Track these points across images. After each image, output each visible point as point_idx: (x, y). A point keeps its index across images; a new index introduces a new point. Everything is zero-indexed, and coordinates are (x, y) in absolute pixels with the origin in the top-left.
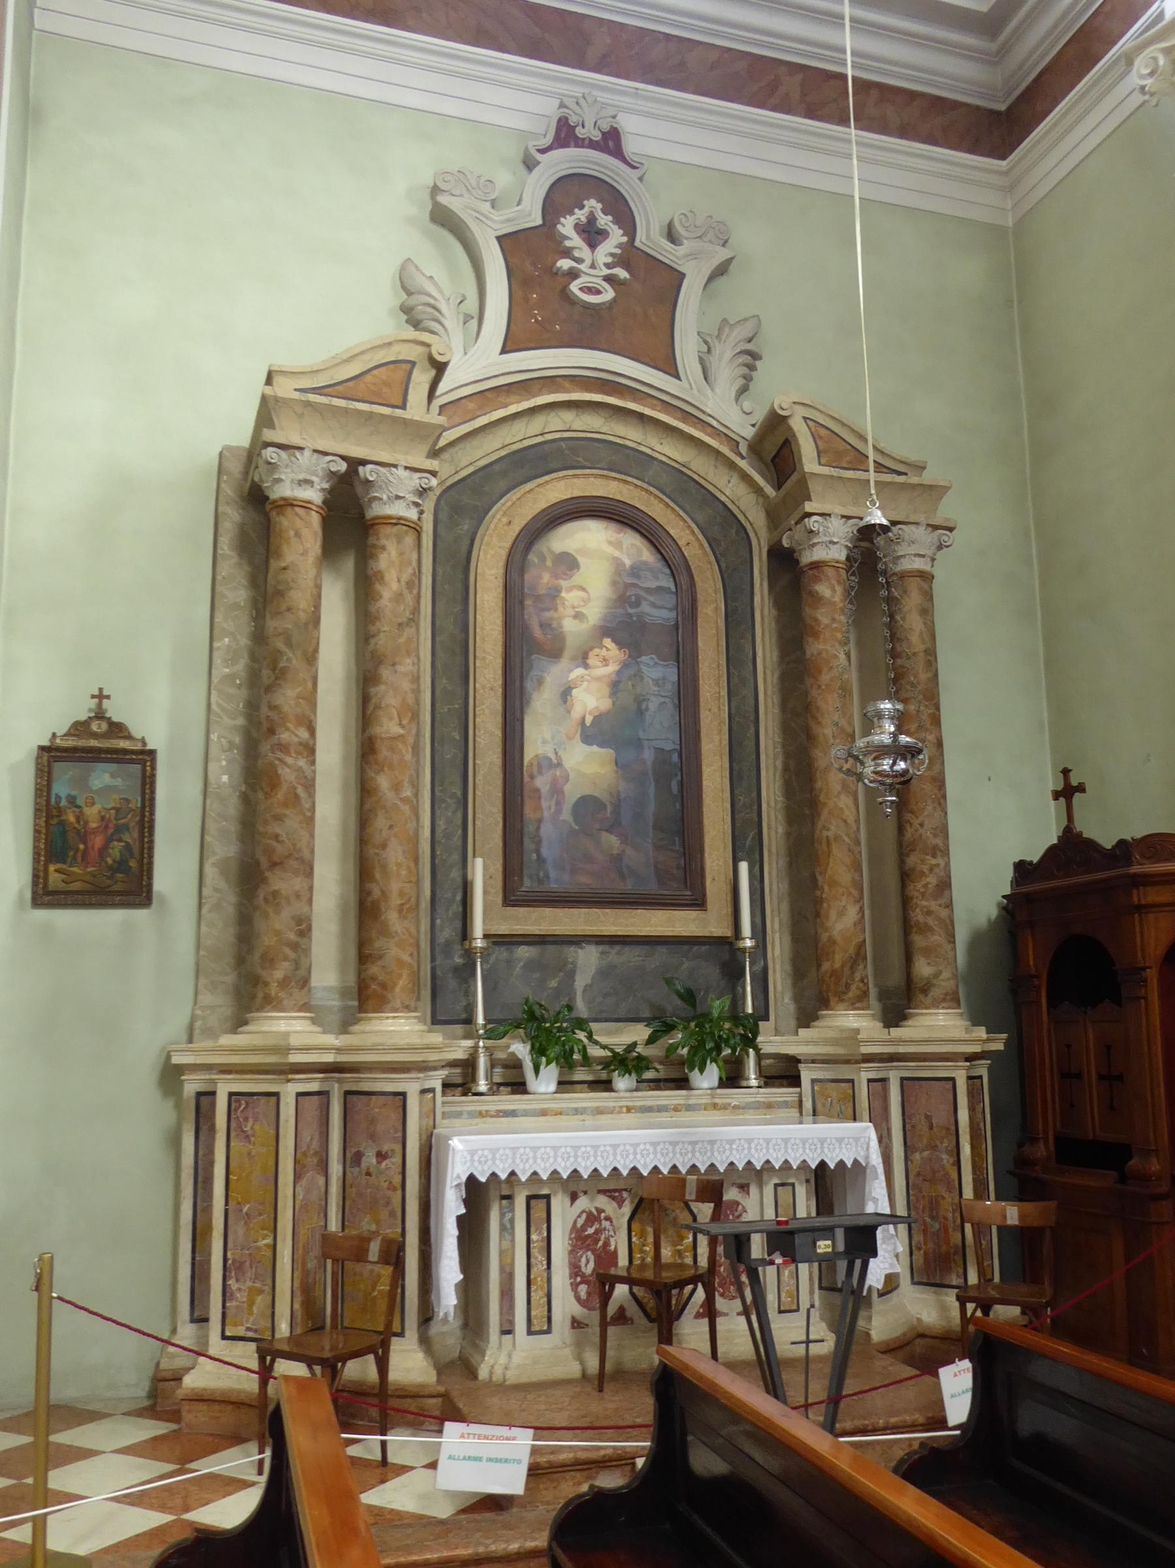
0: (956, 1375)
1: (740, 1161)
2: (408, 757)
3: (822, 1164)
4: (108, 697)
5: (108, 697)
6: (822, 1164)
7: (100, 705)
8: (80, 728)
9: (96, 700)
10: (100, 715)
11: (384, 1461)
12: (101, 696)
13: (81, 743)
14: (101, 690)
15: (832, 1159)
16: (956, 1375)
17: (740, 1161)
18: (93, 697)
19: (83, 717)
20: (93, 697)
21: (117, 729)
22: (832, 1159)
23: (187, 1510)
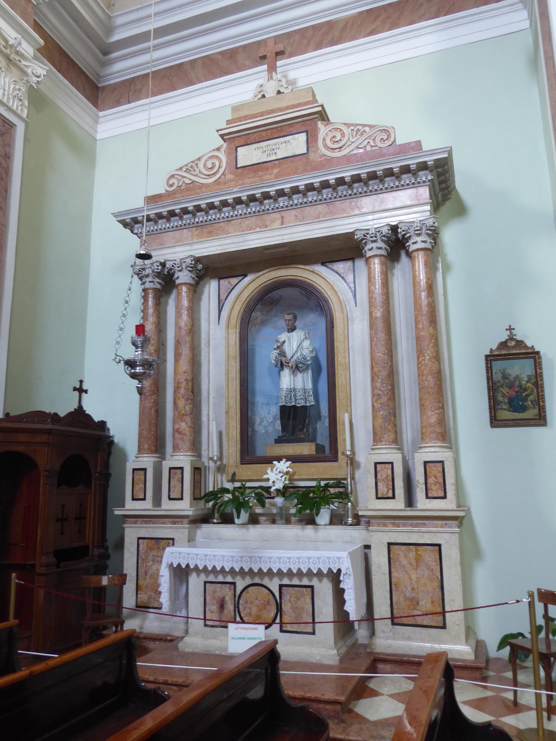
0: (236, 629)
1: (265, 567)
2: (375, 404)
3: (179, 565)
4: (514, 329)
5: (514, 329)
6: (179, 565)
7: (511, 333)
8: (503, 345)
9: (508, 331)
10: (511, 338)
11: (515, 703)
12: (510, 329)
13: (503, 352)
14: (510, 326)
15: (275, 568)
16: (236, 629)
17: (304, 568)
18: (507, 330)
19: (504, 340)
20: (507, 330)
21: (520, 343)
22: (275, 568)
23: (500, 716)
